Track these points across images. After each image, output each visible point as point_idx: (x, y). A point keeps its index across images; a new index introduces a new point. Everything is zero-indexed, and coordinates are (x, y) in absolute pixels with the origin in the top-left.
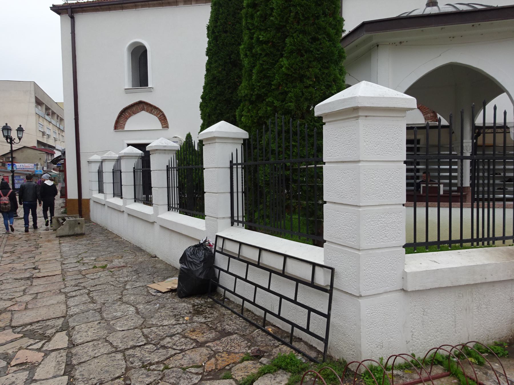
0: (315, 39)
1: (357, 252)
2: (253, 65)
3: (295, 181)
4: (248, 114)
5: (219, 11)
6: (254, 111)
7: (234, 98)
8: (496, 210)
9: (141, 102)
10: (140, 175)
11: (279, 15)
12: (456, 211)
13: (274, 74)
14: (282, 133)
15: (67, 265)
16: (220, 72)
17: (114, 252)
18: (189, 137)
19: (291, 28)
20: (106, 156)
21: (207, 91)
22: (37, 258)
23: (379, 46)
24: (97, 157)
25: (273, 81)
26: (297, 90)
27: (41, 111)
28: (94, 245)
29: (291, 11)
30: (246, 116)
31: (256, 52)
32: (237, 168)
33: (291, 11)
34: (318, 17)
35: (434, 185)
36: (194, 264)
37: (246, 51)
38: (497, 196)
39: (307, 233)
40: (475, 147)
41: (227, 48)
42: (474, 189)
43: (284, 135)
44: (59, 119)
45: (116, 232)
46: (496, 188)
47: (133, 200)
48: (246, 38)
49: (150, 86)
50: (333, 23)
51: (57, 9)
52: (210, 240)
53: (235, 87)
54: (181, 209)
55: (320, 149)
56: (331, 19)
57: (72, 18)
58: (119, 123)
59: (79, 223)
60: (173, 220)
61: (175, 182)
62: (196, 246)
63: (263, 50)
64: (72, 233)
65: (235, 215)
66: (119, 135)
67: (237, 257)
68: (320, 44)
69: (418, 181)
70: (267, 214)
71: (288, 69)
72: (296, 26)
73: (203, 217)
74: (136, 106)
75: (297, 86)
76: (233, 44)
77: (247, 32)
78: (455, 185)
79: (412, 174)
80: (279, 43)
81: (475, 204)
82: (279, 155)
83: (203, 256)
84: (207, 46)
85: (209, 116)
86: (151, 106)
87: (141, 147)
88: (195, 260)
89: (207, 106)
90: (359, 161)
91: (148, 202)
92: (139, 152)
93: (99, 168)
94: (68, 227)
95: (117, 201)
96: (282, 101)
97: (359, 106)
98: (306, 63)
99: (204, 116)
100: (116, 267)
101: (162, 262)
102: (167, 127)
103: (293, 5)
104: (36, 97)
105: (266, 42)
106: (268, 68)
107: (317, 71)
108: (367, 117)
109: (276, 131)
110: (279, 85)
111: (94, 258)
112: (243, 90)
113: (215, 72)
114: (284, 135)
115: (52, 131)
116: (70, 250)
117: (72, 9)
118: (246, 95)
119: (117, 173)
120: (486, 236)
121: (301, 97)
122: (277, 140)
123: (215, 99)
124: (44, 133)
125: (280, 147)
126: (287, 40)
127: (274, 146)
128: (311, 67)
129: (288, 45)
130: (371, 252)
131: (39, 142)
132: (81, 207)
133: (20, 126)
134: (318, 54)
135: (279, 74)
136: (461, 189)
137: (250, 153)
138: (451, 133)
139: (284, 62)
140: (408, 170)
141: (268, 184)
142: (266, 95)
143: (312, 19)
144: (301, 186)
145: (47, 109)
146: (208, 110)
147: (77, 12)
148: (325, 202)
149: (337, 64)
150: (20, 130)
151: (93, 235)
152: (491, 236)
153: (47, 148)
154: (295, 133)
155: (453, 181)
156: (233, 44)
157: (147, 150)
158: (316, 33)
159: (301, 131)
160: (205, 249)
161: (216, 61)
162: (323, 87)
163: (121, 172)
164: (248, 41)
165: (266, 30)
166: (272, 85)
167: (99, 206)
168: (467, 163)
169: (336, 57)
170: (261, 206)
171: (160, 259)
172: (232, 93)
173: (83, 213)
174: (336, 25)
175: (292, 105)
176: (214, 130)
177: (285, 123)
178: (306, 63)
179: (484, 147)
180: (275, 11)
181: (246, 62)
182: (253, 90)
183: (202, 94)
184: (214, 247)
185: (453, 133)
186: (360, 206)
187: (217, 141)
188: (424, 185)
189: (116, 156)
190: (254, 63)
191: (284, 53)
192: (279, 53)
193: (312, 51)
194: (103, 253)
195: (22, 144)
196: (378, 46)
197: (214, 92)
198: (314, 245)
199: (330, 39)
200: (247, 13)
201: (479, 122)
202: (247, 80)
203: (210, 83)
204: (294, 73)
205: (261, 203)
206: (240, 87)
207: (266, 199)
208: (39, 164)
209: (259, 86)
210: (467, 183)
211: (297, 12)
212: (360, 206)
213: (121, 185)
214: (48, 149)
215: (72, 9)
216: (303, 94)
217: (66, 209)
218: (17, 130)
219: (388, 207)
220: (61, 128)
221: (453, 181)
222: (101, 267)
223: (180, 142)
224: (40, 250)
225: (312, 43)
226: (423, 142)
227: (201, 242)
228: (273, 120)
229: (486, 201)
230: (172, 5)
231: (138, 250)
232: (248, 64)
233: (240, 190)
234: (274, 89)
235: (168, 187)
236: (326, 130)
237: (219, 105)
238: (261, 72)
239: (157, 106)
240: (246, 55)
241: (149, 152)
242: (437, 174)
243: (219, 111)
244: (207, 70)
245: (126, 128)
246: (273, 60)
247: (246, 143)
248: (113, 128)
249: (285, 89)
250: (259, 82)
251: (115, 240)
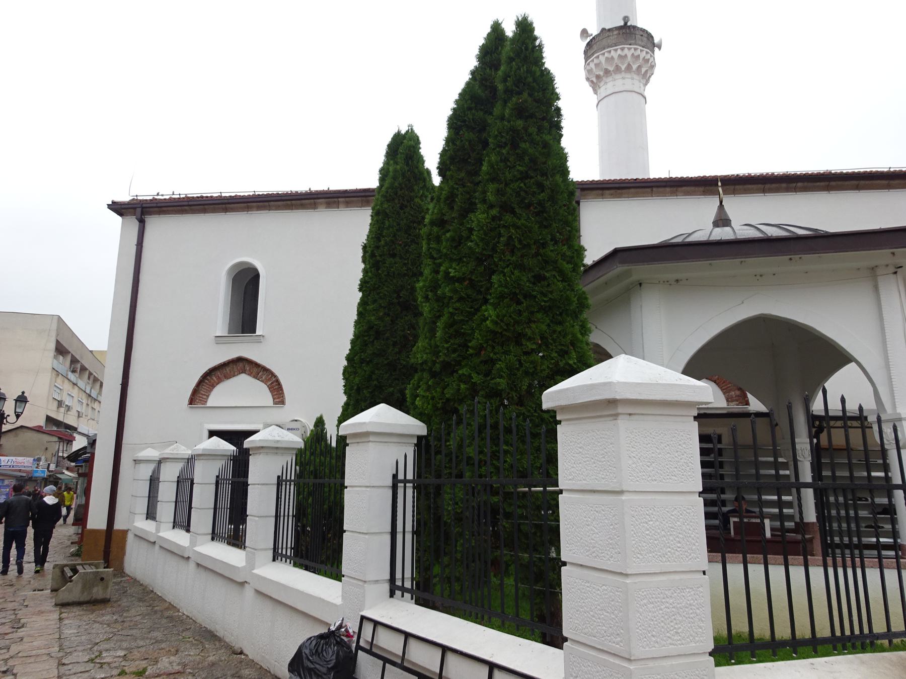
0: (539, 278)
1: (625, 664)
2: (438, 314)
3: (508, 516)
4: (428, 394)
5: (383, 223)
6: (438, 389)
7: (402, 362)
8: (868, 571)
9: (240, 360)
10: (227, 489)
11: (482, 240)
12: (797, 573)
13: (472, 329)
14: (485, 428)
15: (70, 667)
16: (380, 319)
17: (161, 641)
18: (320, 422)
19: (500, 260)
20: (168, 451)
21: (357, 348)
22: (14, 649)
23: (643, 286)
24: (152, 453)
25: (470, 341)
26: (511, 358)
27: (63, 364)
28: (126, 625)
29: (500, 235)
30: (424, 396)
31: (444, 294)
32: (405, 487)
33: (500, 235)
34: (544, 245)
35: (754, 520)
36: (315, 673)
37: (427, 291)
38: (865, 540)
39: (532, 620)
40: (817, 452)
41: (395, 281)
42: (825, 526)
43: (488, 431)
44: (92, 379)
45: (169, 598)
46: (864, 525)
47: (210, 537)
48: (427, 271)
50: (569, 253)
51: (118, 208)
52: (349, 625)
53: (406, 344)
54: (297, 559)
55: (552, 459)
56: (565, 248)
57: (142, 222)
58: (198, 396)
59: (102, 579)
60: (283, 582)
61: (290, 508)
62: (321, 637)
63: (455, 291)
64: (87, 599)
65: (398, 575)
67: (399, 661)
68: (548, 285)
69: (725, 509)
70: (457, 574)
71: (496, 323)
72: (508, 257)
73: (337, 576)
74: (231, 365)
75: (510, 351)
76: (405, 275)
77: (429, 261)
78: (791, 518)
79: (713, 496)
80: (481, 281)
81: (830, 560)
82: (480, 467)
83: (334, 657)
84: (361, 275)
85: (359, 390)
86: (257, 365)
87: (236, 437)
88: (317, 666)
89: (355, 373)
90: (621, 492)
91: (237, 540)
92: (228, 447)
93: (154, 472)
94: (80, 585)
95: (180, 538)
96: (486, 375)
97: (618, 397)
98: (525, 314)
99: (349, 390)
100: (164, 674)
101: (252, 664)
103: (504, 226)
104: (58, 342)
105: (460, 280)
106: (462, 320)
107: (544, 327)
108: (633, 417)
109: (475, 426)
110: (481, 348)
111: (122, 653)
112: (419, 353)
113: (373, 318)
114: (488, 431)
115: (76, 399)
116: (78, 635)
117: (143, 208)
118: (425, 362)
119: (185, 484)
120: (857, 632)
121: (518, 369)
122: (477, 439)
123: (371, 361)
124: (60, 404)
125: (481, 452)
126: (495, 278)
127: (471, 451)
128: (534, 322)
129: (496, 286)
130: (651, 664)
131: (49, 419)
132: (109, 545)
133: (23, 393)
134: (545, 302)
135: (481, 330)
136: (802, 527)
137: (428, 460)
138: (774, 426)
139: (490, 312)
140: (706, 504)
141: (461, 520)
142: (459, 363)
143: (534, 247)
144: (519, 525)
145: (74, 361)
146: (357, 380)
147: (151, 213)
148: (564, 564)
149: (577, 317)
150: (22, 400)
151: (124, 602)
152: (866, 631)
153: (63, 430)
154: (508, 430)
155: (785, 510)
156: (405, 275)
157: (246, 446)
158: (541, 269)
159: (517, 426)
160: (338, 643)
161: (375, 301)
162: (554, 355)
163: (192, 483)
164: (430, 277)
165: (460, 260)
166: (468, 347)
167: (144, 545)
168: (809, 495)
169: (574, 306)
170: (446, 560)
171: (250, 657)
172: (400, 352)
173: (111, 557)
174: (573, 257)
175: (502, 383)
176: (367, 421)
177: (491, 411)
178: (525, 314)
179: (832, 450)
180: (475, 233)
181: (426, 309)
182: (436, 353)
183: (348, 352)
184: (355, 639)
185: (777, 425)
186: (627, 575)
187: (371, 438)
188: (736, 520)
189: (186, 452)
190: (439, 311)
191: (489, 297)
192: (481, 297)
193: (535, 297)
194: (141, 643)
195: (20, 423)
196: (640, 284)
197: (370, 350)
198: (544, 642)
199: (565, 278)
200: (430, 234)
201: (818, 408)
202: (426, 338)
203: (364, 336)
204: (505, 330)
205: (446, 554)
206: (414, 349)
207: (456, 546)
208: (43, 458)
209: (447, 349)
210: (811, 516)
211: (510, 237)
212: (627, 575)
213: (190, 508)
214: (65, 432)
215: (143, 208)
216: (521, 364)
217: (80, 548)
218: (16, 401)
219: (677, 577)
220: (94, 394)
221: (785, 510)
222: (134, 673)
223: (303, 429)
224: (21, 633)
225: (534, 284)
226: (726, 439)
227: (333, 628)
228: (470, 405)
229: (846, 545)
230: (307, 208)
231: (209, 636)
232: (430, 312)
233: (409, 527)
234: (471, 355)
235: (277, 516)
236: (562, 431)
237: (377, 372)
238: (451, 326)
239: (268, 367)
240: (427, 298)
241: (248, 450)
242: (756, 497)
243: (375, 382)
244: (360, 314)
245: (210, 403)
246: (471, 308)
247: (421, 444)
248: (187, 402)
249: (492, 355)
250: (447, 342)
251: (167, 614)
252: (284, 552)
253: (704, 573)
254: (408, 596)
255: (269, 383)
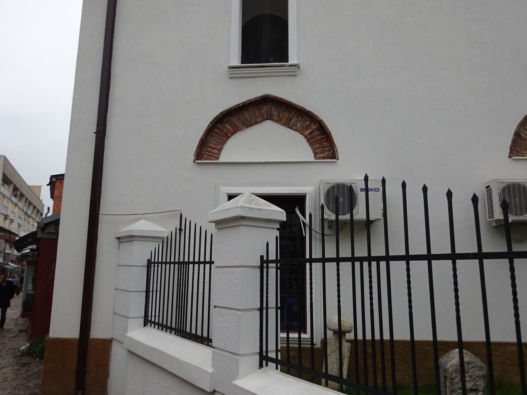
49: (292, 60)
58: (208, 148)
66: (208, 174)
92: (279, 213)
102: (333, 156)
124: (6, 217)
145: (16, 189)
239: (308, 108)
248: (193, 158)
252: (153, 320)
253: (215, 307)
254: (173, 332)
255: (307, 132)
